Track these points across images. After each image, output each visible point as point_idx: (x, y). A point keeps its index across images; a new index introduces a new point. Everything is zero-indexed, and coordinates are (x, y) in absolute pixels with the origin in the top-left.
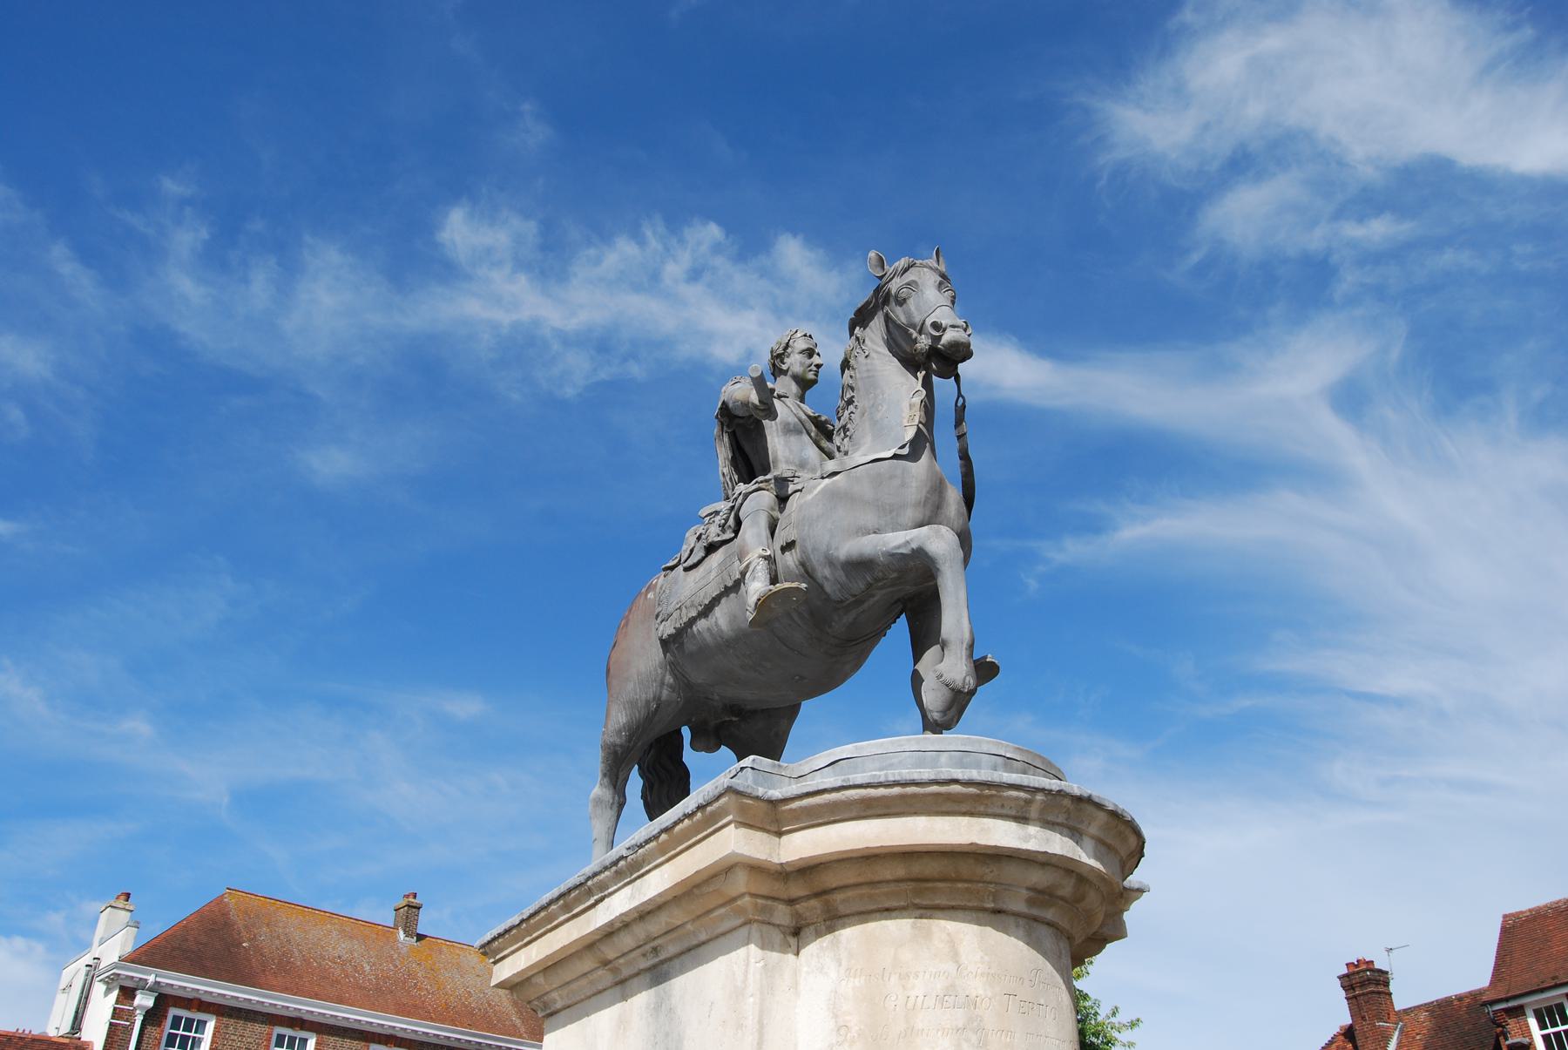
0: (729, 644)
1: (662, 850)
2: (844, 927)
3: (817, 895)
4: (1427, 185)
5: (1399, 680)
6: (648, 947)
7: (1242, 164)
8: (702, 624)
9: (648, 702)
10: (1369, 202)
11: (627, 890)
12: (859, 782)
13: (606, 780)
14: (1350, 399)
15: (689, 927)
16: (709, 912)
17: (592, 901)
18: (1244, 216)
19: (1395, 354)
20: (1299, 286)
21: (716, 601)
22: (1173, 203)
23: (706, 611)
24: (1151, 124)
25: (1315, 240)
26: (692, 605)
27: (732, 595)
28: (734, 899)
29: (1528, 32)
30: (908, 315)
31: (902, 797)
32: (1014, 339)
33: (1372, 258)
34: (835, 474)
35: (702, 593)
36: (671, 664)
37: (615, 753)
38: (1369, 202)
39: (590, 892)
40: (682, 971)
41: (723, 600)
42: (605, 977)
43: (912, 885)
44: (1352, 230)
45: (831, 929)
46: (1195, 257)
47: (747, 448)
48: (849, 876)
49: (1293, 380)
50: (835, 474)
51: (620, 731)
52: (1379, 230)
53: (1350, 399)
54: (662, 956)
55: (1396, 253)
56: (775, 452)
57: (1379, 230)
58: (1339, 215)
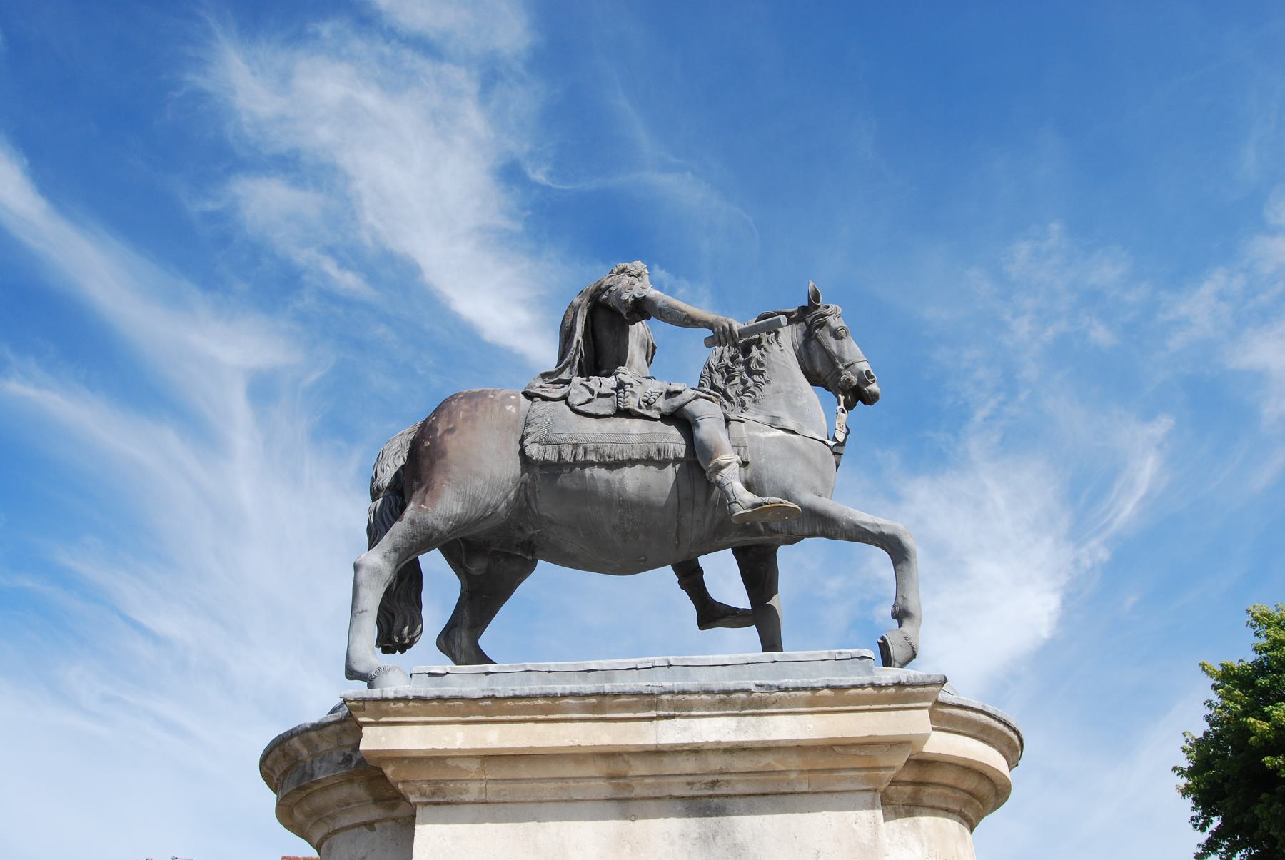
0: (588, 494)
1: (810, 703)
2: (921, 814)
3: (913, 783)
4: (397, 276)
5: (168, 623)
6: (710, 779)
7: (289, 165)
8: (601, 473)
9: (488, 506)
10: (350, 256)
11: (732, 722)
12: (990, 711)
13: (393, 556)
14: (263, 389)
15: (793, 776)
16: (838, 770)
17: (653, 714)
18: (264, 202)
19: (313, 377)
20: (268, 282)
21: (631, 463)
22: (220, 153)
23: (614, 465)
24: (248, 82)
25: (303, 256)
26: (596, 450)
27: (653, 468)
28: (878, 768)
29: (518, 227)
30: (841, 349)
31: (1001, 733)
32: (26, 162)
33: (330, 297)
34: (793, 432)
35: (619, 447)
36: (524, 484)
37: (431, 536)
38: (350, 256)
39: (656, 706)
40: (751, 811)
41: (639, 467)
42: (604, 788)
43: (967, 797)
44: (329, 266)
45: (910, 814)
46: (210, 206)
47: (605, 335)
48: (949, 777)
49: (225, 349)
50: (793, 432)
51: (448, 519)
52: (349, 281)
53: (263, 389)
54: (718, 791)
55: (348, 302)
56: (633, 356)
57: (349, 281)
58: (331, 251)
